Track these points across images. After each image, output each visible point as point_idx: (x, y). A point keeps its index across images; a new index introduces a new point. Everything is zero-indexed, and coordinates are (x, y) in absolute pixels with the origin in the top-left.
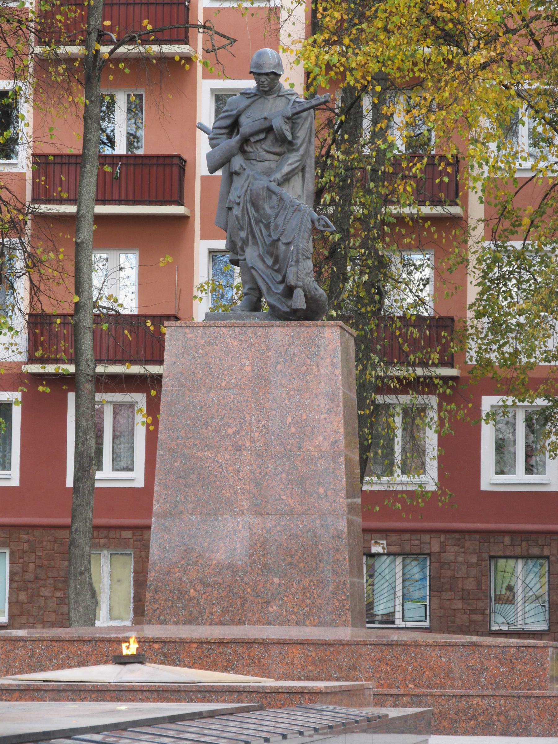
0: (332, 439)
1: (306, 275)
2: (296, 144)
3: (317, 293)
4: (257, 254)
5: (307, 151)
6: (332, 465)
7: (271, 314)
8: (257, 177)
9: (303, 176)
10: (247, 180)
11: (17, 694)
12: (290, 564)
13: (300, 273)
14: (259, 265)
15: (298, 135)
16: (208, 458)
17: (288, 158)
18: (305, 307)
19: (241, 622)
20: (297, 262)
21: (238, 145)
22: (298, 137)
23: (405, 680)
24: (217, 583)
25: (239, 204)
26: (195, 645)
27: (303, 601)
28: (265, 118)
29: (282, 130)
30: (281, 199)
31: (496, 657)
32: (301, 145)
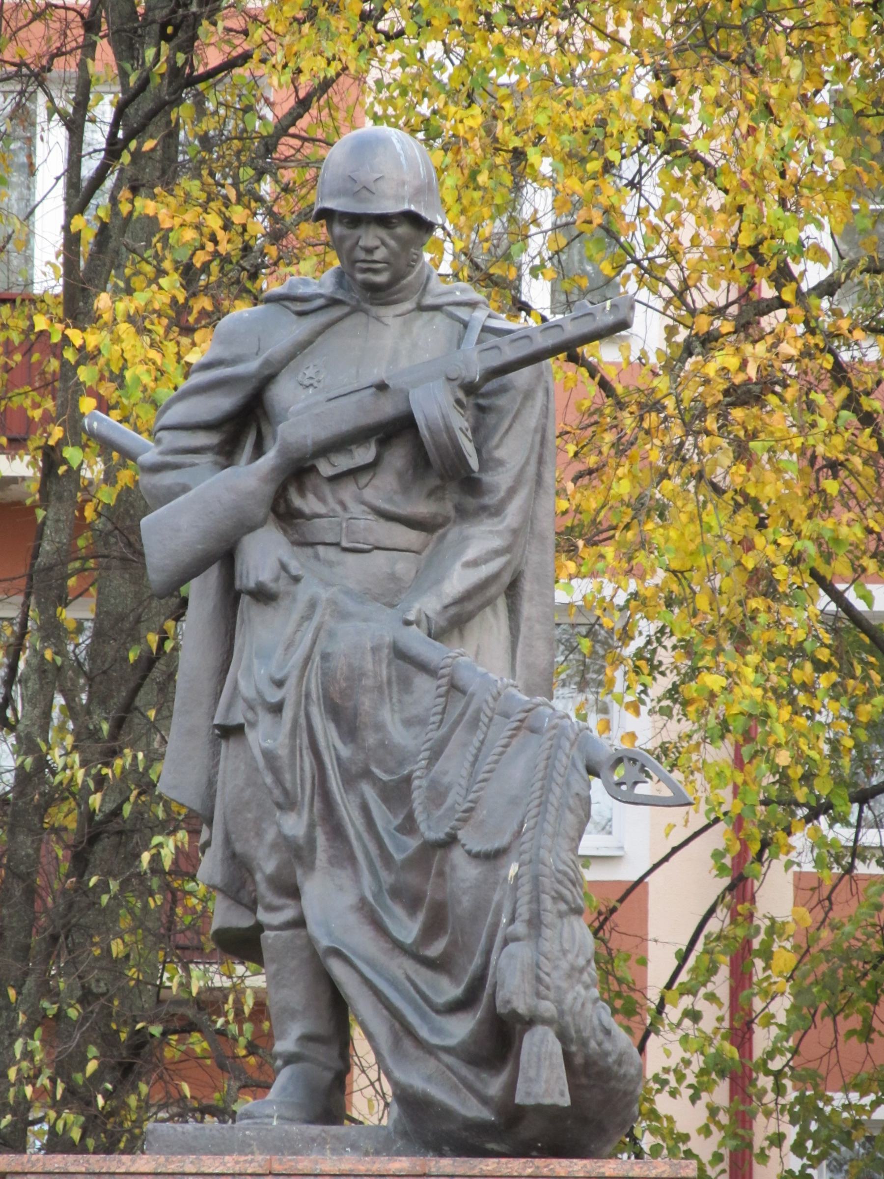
1: (569, 976)
2: (492, 490)
3: (608, 1046)
4: (350, 898)
5: (529, 518)
7: (405, 1134)
8: (351, 606)
9: (513, 611)
10: (307, 617)
13: (546, 966)
14: (361, 940)
15: (500, 454)
17: (464, 541)
18: (565, 1101)
20: (536, 923)
21: (269, 490)
22: (500, 463)
25: (277, 709)
28: (382, 387)
29: (449, 430)
30: (455, 688)
32: (512, 492)
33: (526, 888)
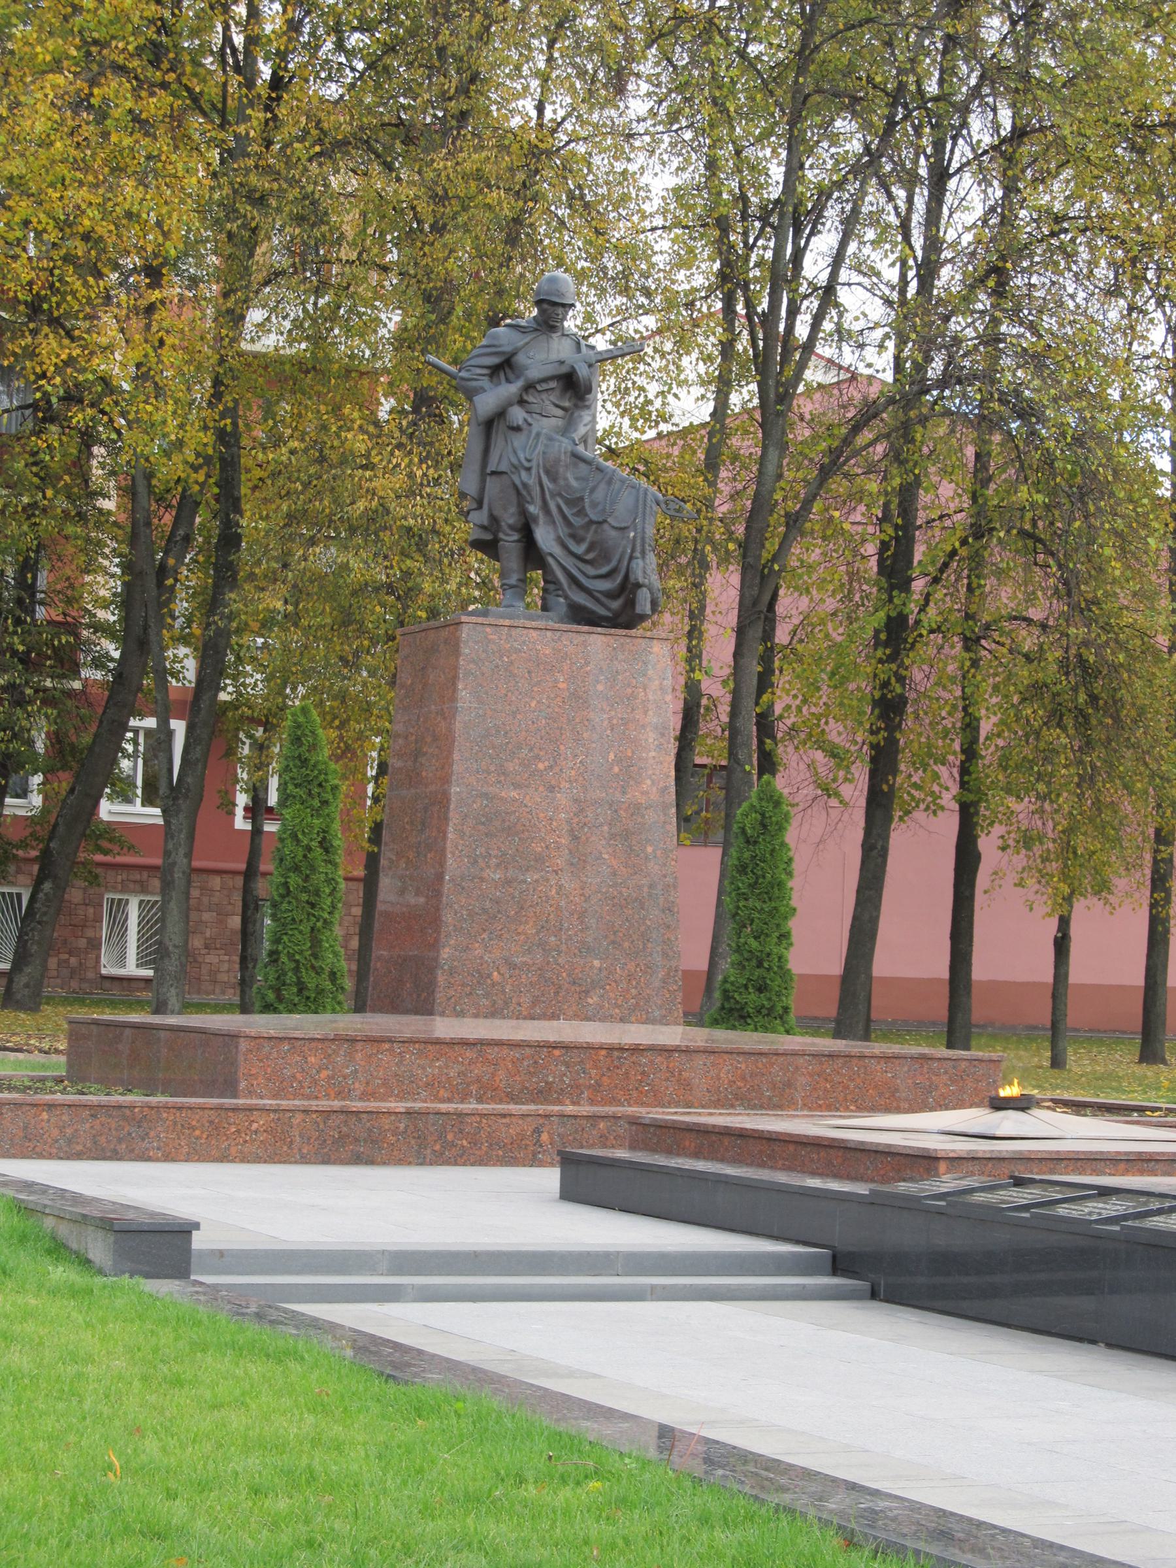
0: (662, 785)
6: (662, 818)
11: (1122, 1166)
12: (613, 942)
16: (515, 800)
19: (554, 1017)
23: (846, 1100)
24: (525, 963)
26: (604, 1052)
27: (628, 991)
31: (946, 1073)
33: (638, 542)
